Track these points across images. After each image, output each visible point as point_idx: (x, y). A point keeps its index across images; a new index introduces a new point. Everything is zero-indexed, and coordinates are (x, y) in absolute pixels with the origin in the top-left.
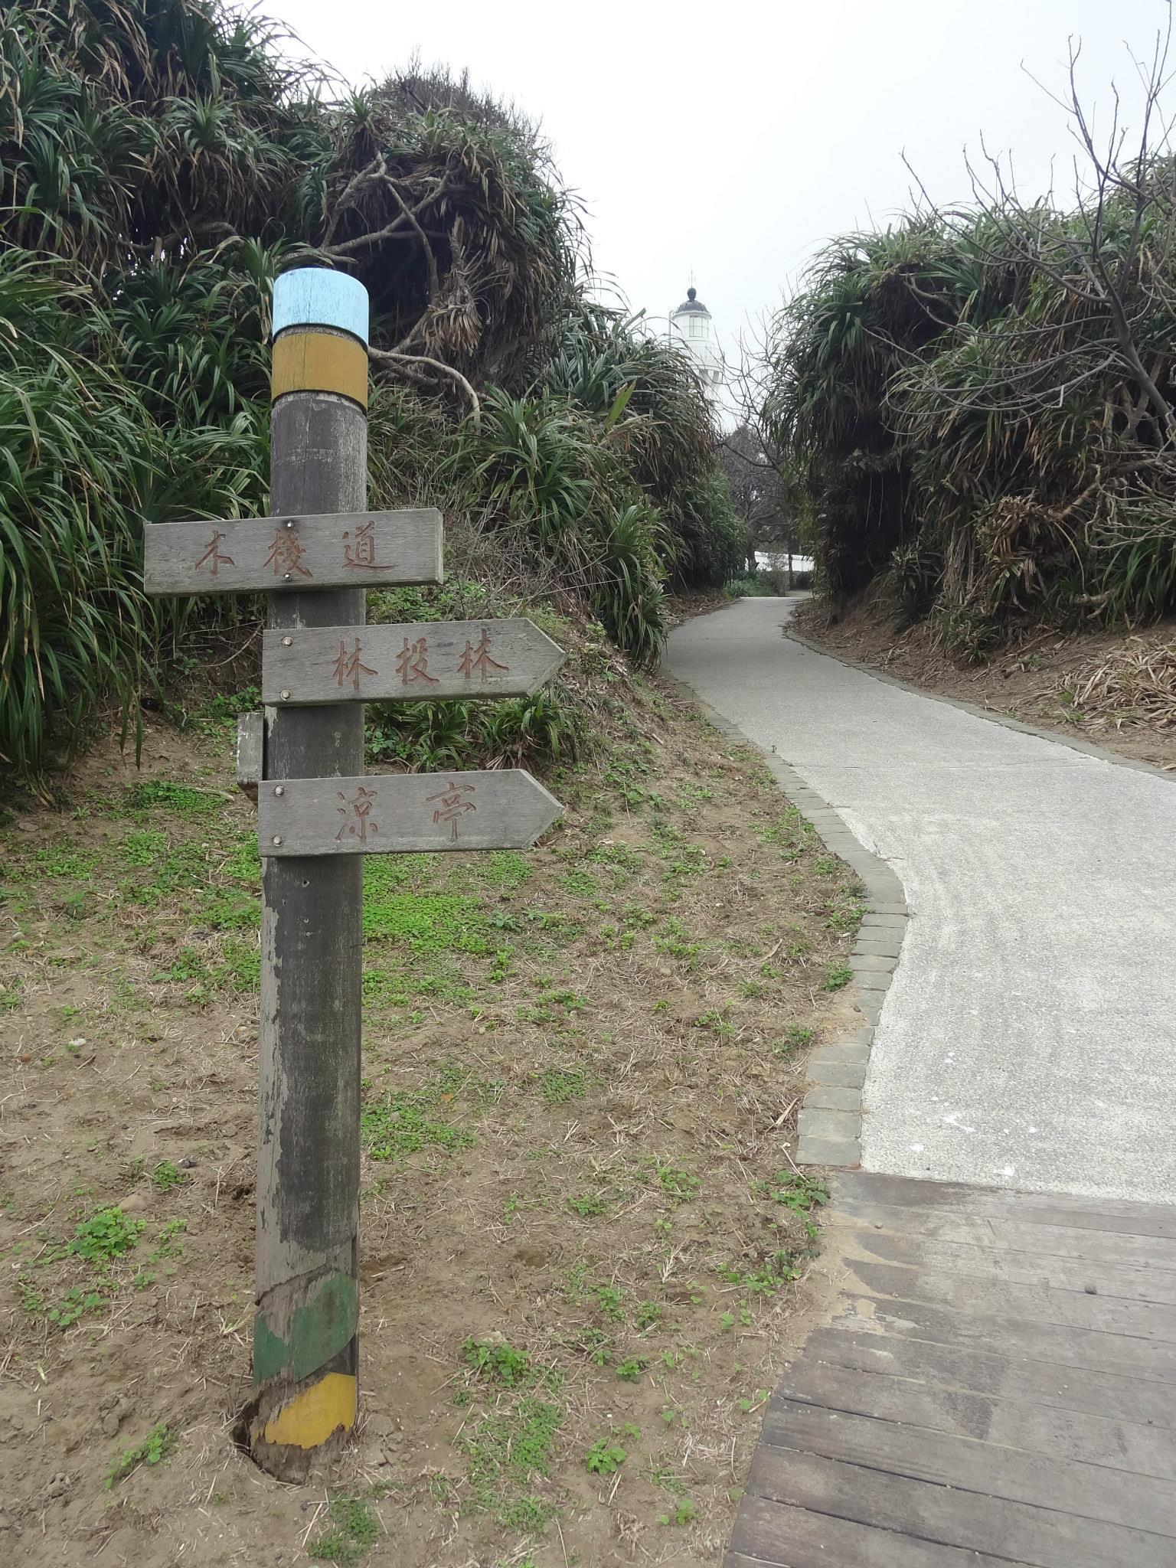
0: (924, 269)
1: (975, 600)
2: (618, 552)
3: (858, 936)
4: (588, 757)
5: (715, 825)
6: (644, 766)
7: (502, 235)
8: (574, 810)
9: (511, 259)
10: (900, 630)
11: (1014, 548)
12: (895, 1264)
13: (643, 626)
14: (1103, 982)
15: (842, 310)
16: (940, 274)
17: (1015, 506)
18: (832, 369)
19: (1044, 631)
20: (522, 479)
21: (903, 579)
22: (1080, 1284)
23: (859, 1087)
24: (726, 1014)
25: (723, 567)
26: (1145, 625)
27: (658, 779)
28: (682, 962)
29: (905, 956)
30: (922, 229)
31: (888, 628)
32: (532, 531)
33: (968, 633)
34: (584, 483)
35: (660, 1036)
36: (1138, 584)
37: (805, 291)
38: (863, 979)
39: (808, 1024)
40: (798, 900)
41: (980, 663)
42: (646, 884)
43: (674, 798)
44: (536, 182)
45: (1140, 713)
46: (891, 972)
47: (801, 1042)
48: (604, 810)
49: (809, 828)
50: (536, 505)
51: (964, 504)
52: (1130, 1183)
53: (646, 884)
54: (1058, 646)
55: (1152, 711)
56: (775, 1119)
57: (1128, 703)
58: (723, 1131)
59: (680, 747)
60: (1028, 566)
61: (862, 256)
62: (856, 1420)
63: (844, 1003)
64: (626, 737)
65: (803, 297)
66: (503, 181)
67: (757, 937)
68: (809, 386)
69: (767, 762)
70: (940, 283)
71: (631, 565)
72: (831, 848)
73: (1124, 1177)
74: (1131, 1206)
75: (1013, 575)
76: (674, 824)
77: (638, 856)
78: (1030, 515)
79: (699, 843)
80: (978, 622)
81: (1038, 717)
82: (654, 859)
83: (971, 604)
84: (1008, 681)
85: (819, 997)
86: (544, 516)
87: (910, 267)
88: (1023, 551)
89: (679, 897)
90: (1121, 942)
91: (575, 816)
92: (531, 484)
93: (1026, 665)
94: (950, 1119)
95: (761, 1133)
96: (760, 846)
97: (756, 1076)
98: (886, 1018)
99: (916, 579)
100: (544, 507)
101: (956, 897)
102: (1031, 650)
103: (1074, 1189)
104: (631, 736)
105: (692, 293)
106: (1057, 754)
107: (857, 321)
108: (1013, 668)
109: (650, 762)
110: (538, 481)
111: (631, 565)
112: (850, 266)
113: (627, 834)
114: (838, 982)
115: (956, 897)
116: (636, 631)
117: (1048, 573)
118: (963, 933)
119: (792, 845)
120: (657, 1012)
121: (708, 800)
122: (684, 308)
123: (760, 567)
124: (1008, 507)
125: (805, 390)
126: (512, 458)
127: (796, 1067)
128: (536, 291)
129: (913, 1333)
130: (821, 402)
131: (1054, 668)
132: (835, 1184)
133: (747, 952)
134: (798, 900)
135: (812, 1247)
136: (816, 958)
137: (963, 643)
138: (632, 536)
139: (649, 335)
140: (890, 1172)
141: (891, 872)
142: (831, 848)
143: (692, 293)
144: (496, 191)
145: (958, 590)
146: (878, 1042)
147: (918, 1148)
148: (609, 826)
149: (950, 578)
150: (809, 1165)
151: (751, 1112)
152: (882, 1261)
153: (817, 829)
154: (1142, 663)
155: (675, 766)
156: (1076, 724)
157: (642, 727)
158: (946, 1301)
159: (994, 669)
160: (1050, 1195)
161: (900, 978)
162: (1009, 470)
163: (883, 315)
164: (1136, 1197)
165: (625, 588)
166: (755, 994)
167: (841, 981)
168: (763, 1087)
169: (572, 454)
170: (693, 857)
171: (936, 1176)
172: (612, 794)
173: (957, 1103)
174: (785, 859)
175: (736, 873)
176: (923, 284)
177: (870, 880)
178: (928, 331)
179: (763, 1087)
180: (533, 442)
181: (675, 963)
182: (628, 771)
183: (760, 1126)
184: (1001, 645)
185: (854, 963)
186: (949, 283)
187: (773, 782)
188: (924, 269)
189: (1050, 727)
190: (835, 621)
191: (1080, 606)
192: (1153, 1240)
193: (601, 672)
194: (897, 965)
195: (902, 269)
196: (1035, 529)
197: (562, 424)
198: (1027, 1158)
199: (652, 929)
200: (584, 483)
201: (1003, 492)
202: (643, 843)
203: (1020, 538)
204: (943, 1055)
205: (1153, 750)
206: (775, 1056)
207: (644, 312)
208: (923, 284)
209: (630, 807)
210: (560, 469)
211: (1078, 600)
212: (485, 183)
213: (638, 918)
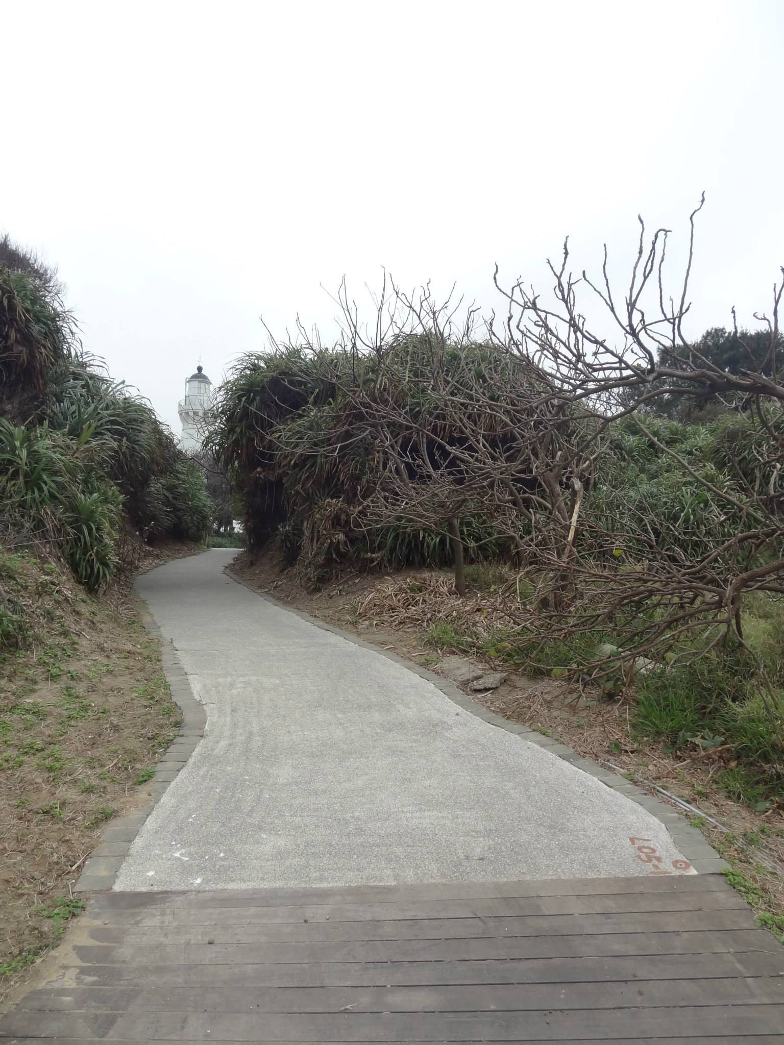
0: (292, 375)
1: (317, 554)
2: (81, 519)
3: (168, 750)
4: (28, 647)
5: (109, 687)
6: (71, 651)
7: (18, 331)
8: (10, 681)
9: (23, 345)
10: (282, 571)
11: (334, 527)
12: (105, 944)
13: (97, 566)
14: (295, 767)
15: (249, 391)
16: (299, 379)
17: (333, 504)
18: (244, 423)
19: (351, 572)
20: (15, 475)
21: (283, 541)
22: (207, 939)
23: (130, 841)
24: (64, 804)
25: (199, 529)
26: (398, 570)
27: (79, 660)
28: (52, 774)
29: (191, 761)
30: (295, 353)
31: (276, 570)
32: (20, 506)
33: (313, 573)
34: (59, 479)
35: (15, 822)
36: (392, 550)
37: (231, 378)
38: (159, 777)
39: (114, 806)
40: (143, 731)
41: (317, 590)
42: (47, 726)
43: (86, 672)
44: (45, 305)
45: (386, 618)
46: (178, 771)
47: (106, 816)
48: (32, 680)
49: (167, 687)
50: (24, 491)
51: (309, 499)
52: (262, 879)
53: (47, 726)
54: (357, 581)
55: (392, 617)
56: (71, 866)
57: (381, 612)
58: (33, 878)
59: (101, 640)
60: (342, 537)
61: (262, 364)
62: (28, 1041)
63: (142, 793)
64: (61, 634)
65: (228, 382)
66: (18, 300)
67: (106, 755)
68: (231, 430)
69: (162, 649)
70: (300, 383)
71: (90, 529)
72: (174, 699)
73: (261, 875)
74: (255, 891)
75: (332, 541)
76: (80, 688)
77: (48, 709)
78: (341, 509)
79: (95, 700)
80: (318, 567)
81: (334, 622)
82: (59, 710)
83: (314, 557)
84: (331, 601)
85: (130, 789)
86: (29, 497)
87: (283, 373)
88: (339, 528)
89: (66, 733)
90: (314, 744)
91: (11, 685)
92: (21, 478)
93: (340, 591)
94: (177, 855)
95: (60, 876)
96: (132, 699)
97: (67, 841)
98: (165, 799)
99: (290, 541)
100: (29, 492)
101: (235, 724)
102: (344, 583)
103: (231, 886)
104: (65, 634)
105: (200, 369)
106: (341, 644)
107: (258, 398)
108: (334, 593)
109: (75, 649)
110: (26, 475)
111: (90, 529)
112: (255, 368)
113: (46, 695)
114: (145, 778)
115: (235, 724)
116: (92, 568)
117: (352, 541)
118: (230, 745)
119: (152, 698)
120: (18, 806)
121: (110, 672)
122: (194, 377)
123: (236, 530)
124: (329, 505)
125: (229, 433)
126: (11, 462)
127: (98, 832)
128: (41, 364)
129: (94, 983)
130: (237, 440)
131: (353, 593)
132: (92, 902)
133: (96, 765)
134: (143, 731)
135: (57, 940)
136: (138, 766)
137: (309, 579)
138: (93, 512)
139: (127, 395)
140: (128, 890)
141: (204, 711)
142: (174, 699)
143: (200, 369)
144: (12, 307)
145: (309, 550)
146: (154, 813)
147: (151, 873)
148: (33, 691)
149: (305, 542)
150: (80, 892)
151: (57, 863)
152: (98, 943)
153: (171, 688)
154: (390, 591)
155: (93, 652)
156: (355, 624)
157: (74, 628)
158: (124, 962)
159: (324, 593)
160: (215, 891)
161: (183, 774)
162: (330, 484)
163: (272, 394)
164: (262, 886)
165: (85, 542)
166: (89, 790)
167: (146, 778)
168: (71, 849)
169: (51, 461)
170: (85, 708)
171: (155, 889)
172: (41, 669)
173: (184, 844)
174: (146, 707)
175: (109, 717)
176: (291, 383)
177: (189, 717)
178: (296, 406)
179: (71, 849)
180: (24, 453)
181: (47, 775)
182: (56, 656)
183: (60, 872)
184: (329, 580)
185: (160, 766)
186: (305, 384)
187: (159, 661)
188: (292, 375)
189: (340, 626)
190: (252, 564)
191: (366, 559)
192: (259, 909)
193: (51, 594)
194: (183, 766)
195: (280, 374)
196: (343, 517)
197: (49, 443)
198: (212, 871)
199: (39, 755)
200: (59, 479)
201: (328, 496)
202: (54, 700)
203: (337, 521)
204: (189, 816)
205: (387, 638)
206: (86, 828)
207: (123, 382)
208: (291, 383)
209: (53, 678)
210: (44, 470)
211: (365, 556)
212: (5, 302)
213: (32, 748)
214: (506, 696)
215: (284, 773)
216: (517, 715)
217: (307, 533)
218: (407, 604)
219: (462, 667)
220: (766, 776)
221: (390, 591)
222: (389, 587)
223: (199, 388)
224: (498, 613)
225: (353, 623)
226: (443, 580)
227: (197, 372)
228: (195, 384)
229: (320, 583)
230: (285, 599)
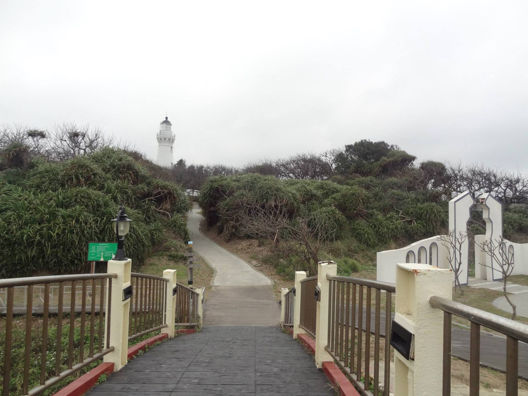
33: (227, 238)
105: (167, 118)
106: (234, 257)
143: (167, 118)
214: (261, 267)
215: (229, 276)
216: (261, 271)
217: (225, 228)
218: (248, 248)
219: (254, 262)
220: (123, 207)
221: (244, 245)
222: (244, 244)
223: (166, 127)
224: (265, 252)
225: (236, 252)
226: (255, 242)
227: (165, 119)
228: (165, 125)
229: (228, 241)
230: (220, 244)
